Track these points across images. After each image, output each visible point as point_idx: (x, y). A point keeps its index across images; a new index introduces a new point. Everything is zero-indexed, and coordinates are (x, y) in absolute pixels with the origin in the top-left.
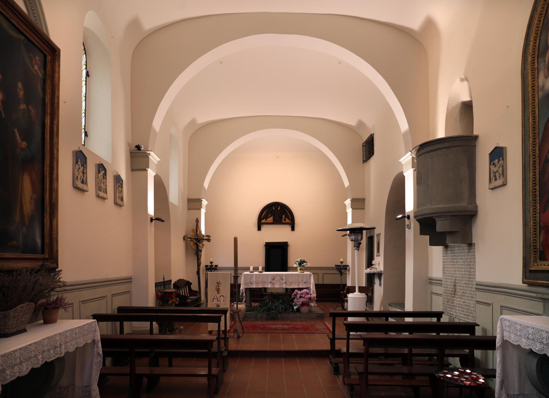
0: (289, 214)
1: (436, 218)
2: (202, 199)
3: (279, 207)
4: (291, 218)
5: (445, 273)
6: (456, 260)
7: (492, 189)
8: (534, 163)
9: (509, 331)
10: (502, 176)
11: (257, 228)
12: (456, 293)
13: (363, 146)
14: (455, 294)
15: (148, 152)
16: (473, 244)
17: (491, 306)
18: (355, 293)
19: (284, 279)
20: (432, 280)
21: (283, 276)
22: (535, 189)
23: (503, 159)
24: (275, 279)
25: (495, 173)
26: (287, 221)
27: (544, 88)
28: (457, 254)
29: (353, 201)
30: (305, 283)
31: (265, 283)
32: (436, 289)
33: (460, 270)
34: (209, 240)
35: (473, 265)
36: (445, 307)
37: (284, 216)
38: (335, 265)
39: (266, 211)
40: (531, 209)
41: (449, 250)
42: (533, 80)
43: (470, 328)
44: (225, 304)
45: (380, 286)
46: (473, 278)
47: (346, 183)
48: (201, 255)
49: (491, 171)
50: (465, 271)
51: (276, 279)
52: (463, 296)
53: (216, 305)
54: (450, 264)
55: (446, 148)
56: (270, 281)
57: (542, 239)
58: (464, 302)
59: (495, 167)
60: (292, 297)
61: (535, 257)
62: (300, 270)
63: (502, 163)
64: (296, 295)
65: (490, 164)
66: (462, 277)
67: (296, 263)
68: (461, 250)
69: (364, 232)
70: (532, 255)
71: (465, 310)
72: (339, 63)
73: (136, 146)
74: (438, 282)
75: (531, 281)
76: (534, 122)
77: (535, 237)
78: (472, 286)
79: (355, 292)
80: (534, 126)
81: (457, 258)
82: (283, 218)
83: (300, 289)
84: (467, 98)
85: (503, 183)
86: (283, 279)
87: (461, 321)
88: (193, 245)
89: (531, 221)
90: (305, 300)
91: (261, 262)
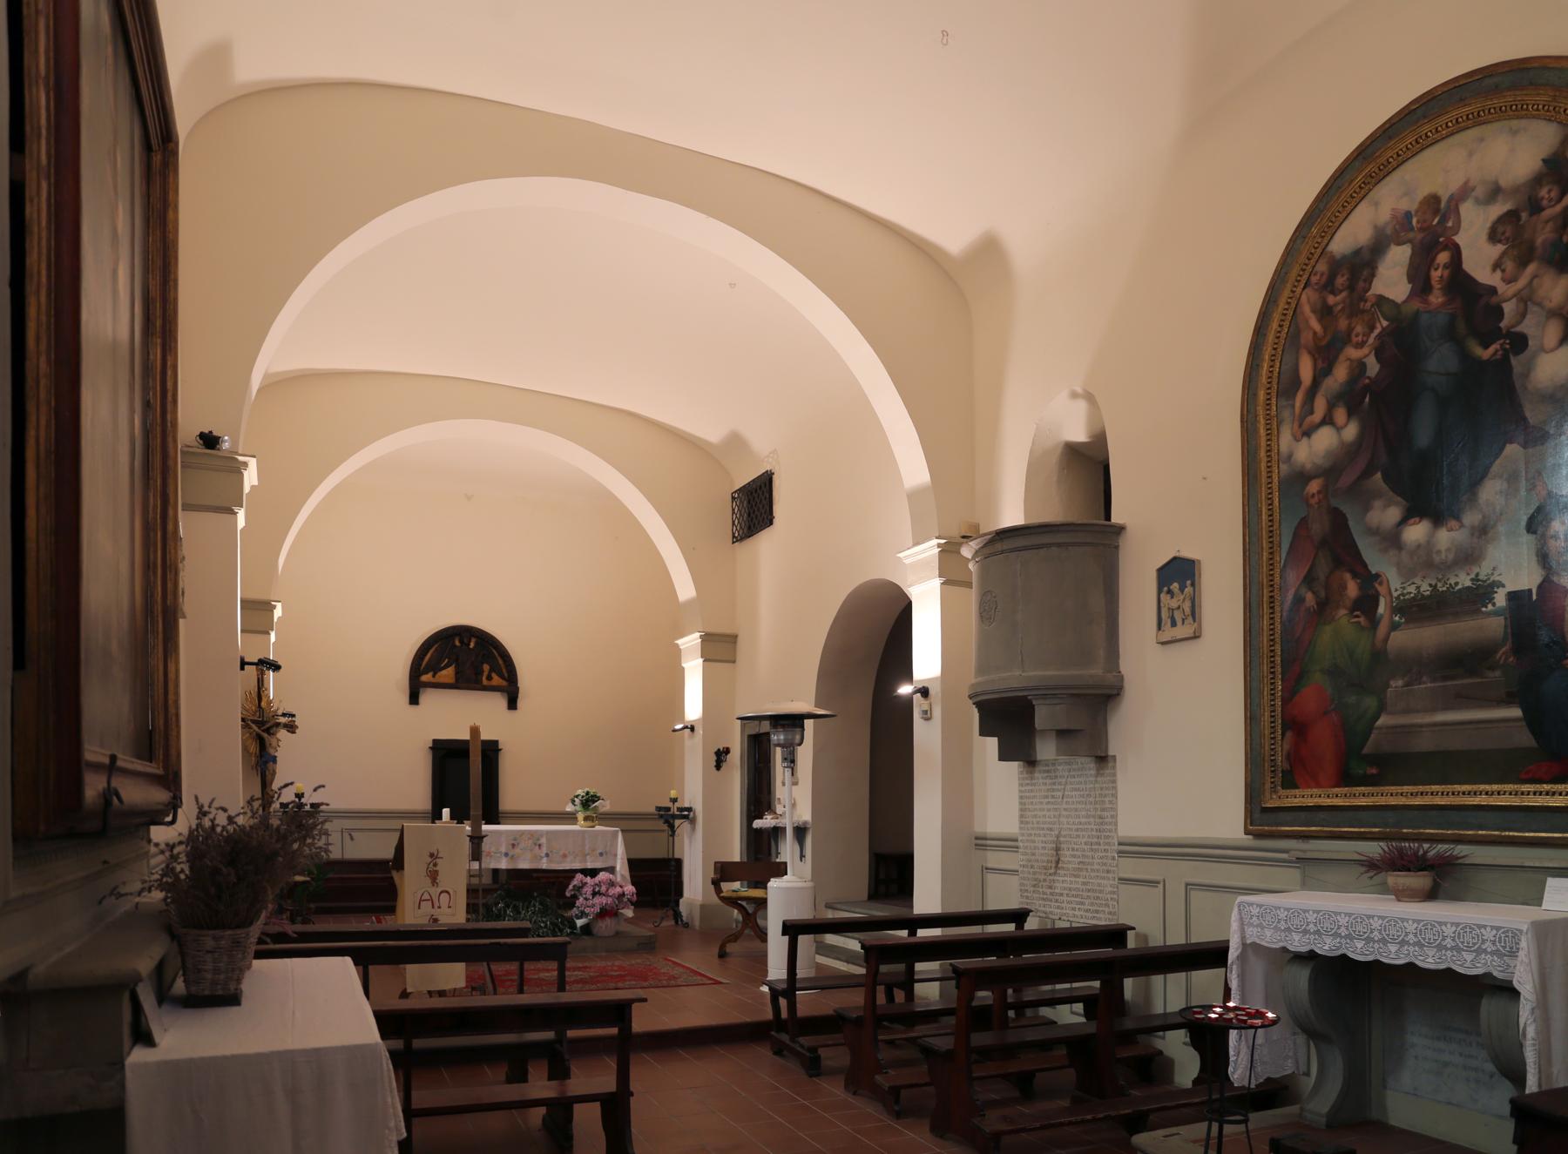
0: (501, 662)
1: (1036, 699)
2: (273, 603)
3: (473, 640)
4: (506, 675)
5: (1027, 823)
6: (1060, 794)
7: (1163, 643)
8: (1272, 600)
9: (1260, 926)
10: (1190, 618)
11: (406, 698)
12: (1060, 865)
13: (733, 498)
14: (1056, 867)
15: (241, 458)
16: (1110, 759)
17: (1161, 886)
18: (785, 877)
19: (545, 845)
20: (986, 839)
21: (542, 836)
22: (1272, 651)
23: (1193, 585)
24: (518, 844)
25: (1171, 610)
26: (496, 680)
27: (1293, 459)
28: (1064, 780)
29: (708, 639)
30: (601, 854)
31: (491, 856)
32: (994, 859)
33: (1073, 813)
34: (291, 728)
35: (1110, 802)
36: (1027, 897)
37: (488, 667)
38: (657, 807)
39: (436, 649)
40: (1266, 689)
41: (1040, 772)
42: (1269, 437)
43: (1116, 935)
44: (454, 915)
45: (801, 860)
46: (1110, 831)
47: (685, 589)
48: (274, 773)
49: (1162, 605)
50: (1088, 816)
51: (522, 845)
52: (1080, 870)
53: (428, 918)
54: (1041, 803)
55: (1059, 545)
56: (503, 850)
57: (1286, 747)
58: (1084, 883)
59: (1172, 597)
60: (568, 894)
61: (1272, 783)
62: (586, 819)
63: (1192, 592)
64: (579, 889)
65: (1160, 591)
66: (1077, 830)
67: (573, 802)
68: (1074, 770)
69: (808, 724)
70: (1269, 780)
71: (1087, 901)
72: (730, 284)
73: (202, 435)
74: (1008, 843)
75: (1266, 828)
76: (1270, 521)
77: (1273, 744)
78: (1106, 847)
79: (786, 874)
80: (1271, 529)
81: (1064, 789)
82: (485, 674)
83: (593, 873)
84: (1079, 435)
85: (1195, 632)
86: (540, 845)
87: (1074, 925)
88: (250, 741)
89: (1266, 714)
90: (610, 900)
91: (415, 789)
